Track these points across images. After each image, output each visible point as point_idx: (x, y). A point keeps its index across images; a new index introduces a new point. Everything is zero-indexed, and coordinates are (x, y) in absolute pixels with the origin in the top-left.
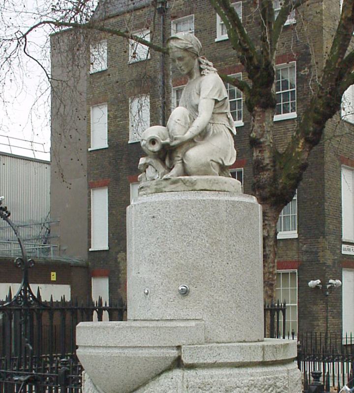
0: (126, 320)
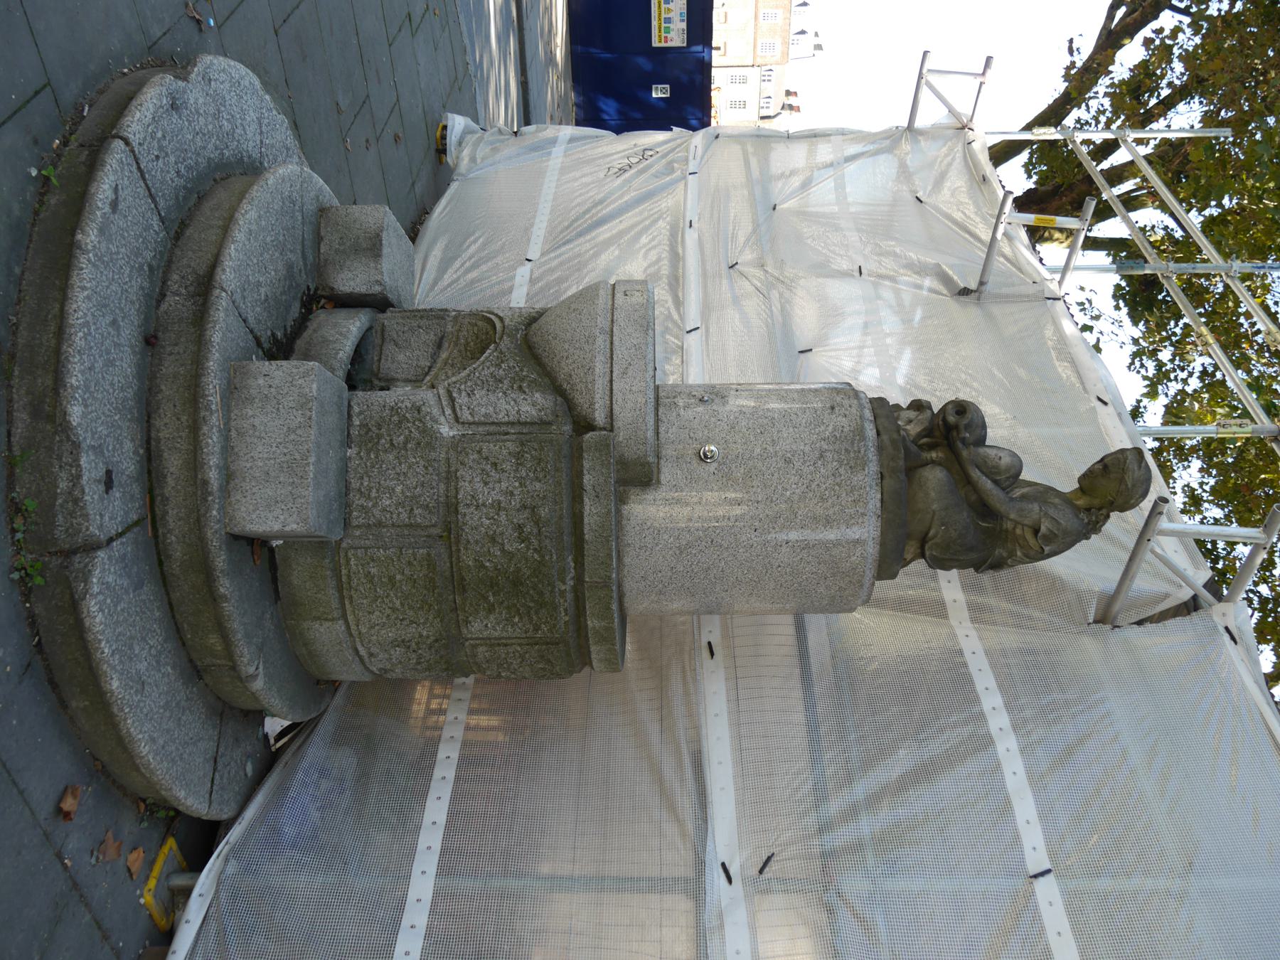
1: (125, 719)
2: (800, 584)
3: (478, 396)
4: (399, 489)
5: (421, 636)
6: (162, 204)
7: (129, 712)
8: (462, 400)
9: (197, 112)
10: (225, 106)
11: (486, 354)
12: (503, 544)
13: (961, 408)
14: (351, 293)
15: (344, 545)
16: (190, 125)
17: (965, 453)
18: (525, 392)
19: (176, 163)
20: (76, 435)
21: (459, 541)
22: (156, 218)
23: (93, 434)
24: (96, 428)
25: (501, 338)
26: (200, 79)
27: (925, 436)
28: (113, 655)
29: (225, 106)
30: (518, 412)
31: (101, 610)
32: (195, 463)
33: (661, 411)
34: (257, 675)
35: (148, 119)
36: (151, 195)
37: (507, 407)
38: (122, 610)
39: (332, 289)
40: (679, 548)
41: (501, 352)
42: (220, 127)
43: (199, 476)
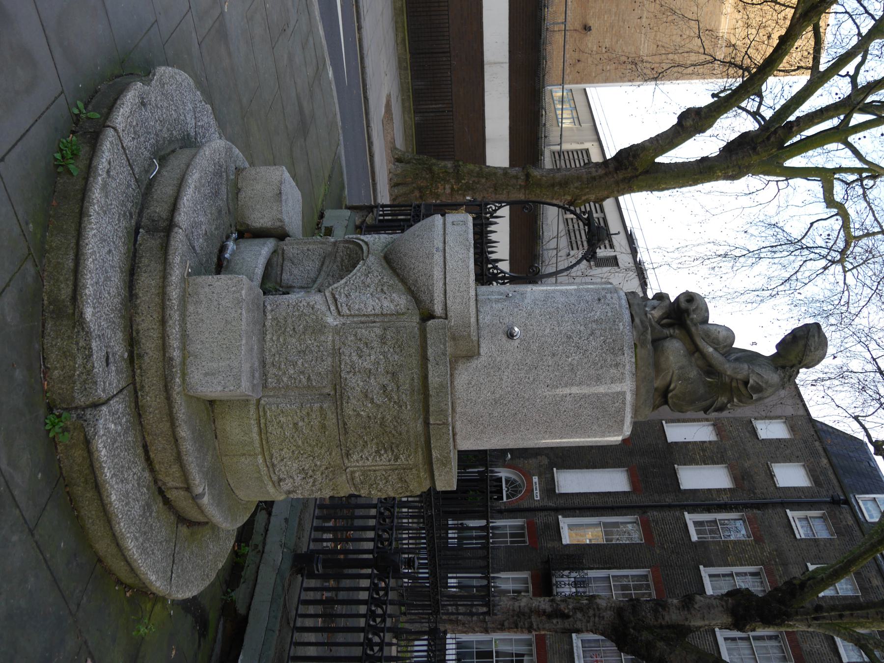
0: (477, 285)
1: (119, 523)
2: (580, 423)
3: (353, 297)
4: (300, 363)
5: (316, 465)
6: (137, 170)
7: (122, 518)
8: (342, 299)
9: (157, 106)
10: (173, 101)
11: (357, 268)
12: (372, 399)
13: (690, 297)
14: (261, 228)
15: (262, 402)
16: (152, 115)
17: (693, 329)
18: (385, 293)
19: (144, 142)
20: (89, 327)
21: (342, 398)
22: (133, 180)
23: (99, 326)
24: (100, 323)
25: (367, 256)
26: (158, 83)
27: (664, 319)
28: (112, 478)
29: (173, 101)
30: (381, 307)
31: (105, 447)
32: (164, 347)
33: (479, 304)
34: (204, 494)
35: (127, 114)
36: (130, 165)
37: (373, 303)
38: (117, 447)
39: (248, 225)
40: (495, 400)
41: (368, 266)
42: (171, 115)
43: (167, 355)
